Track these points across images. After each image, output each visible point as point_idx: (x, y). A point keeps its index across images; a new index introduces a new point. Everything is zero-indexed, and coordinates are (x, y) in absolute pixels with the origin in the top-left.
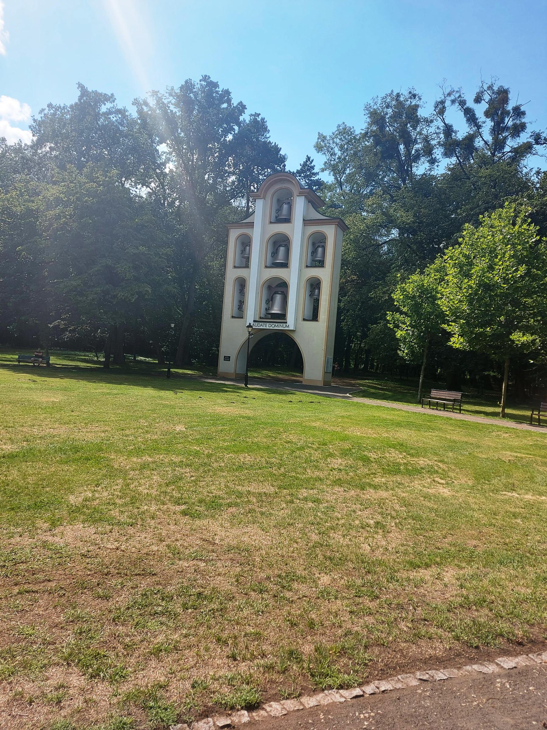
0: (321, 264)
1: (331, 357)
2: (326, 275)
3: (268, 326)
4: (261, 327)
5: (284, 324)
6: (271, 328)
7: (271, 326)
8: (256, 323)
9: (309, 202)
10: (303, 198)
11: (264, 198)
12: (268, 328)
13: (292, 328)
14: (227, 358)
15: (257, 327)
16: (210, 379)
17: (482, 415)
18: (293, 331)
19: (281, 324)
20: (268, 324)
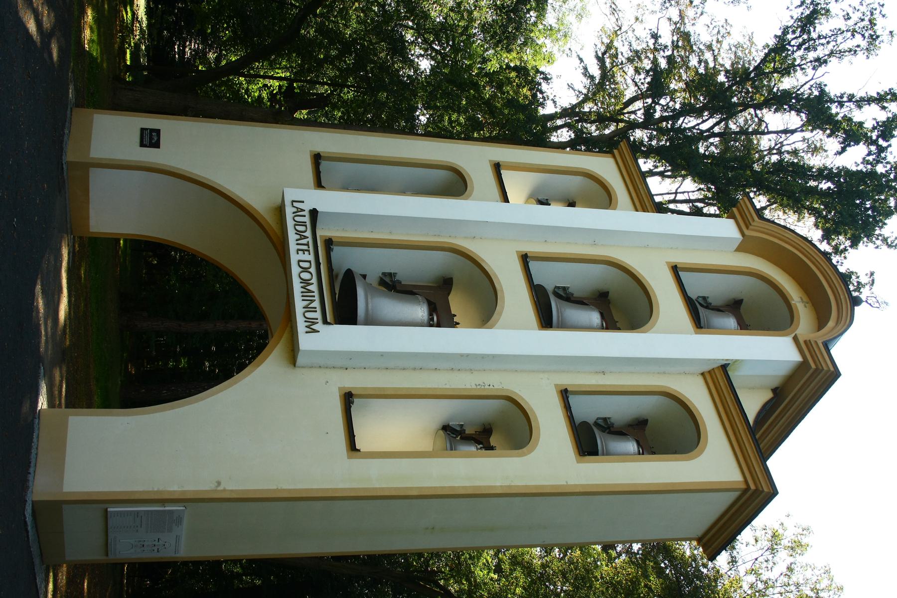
0: (588, 439)
1: (184, 545)
2: (550, 460)
3: (301, 256)
4: (292, 237)
5: (318, 315)
6: (295, 270)
7: (305, 270)
8: (307, 219)
9: (774, 390)
10: (795, 357)
11: (743, 247)
12: (294, 258)
13: (306, 342)
14: (151, 139)
15: (290, 223)
16: (69, 302)
17: (577, 294)
18: (293, 353)
19: (316, 304)
20: (311, 257)
